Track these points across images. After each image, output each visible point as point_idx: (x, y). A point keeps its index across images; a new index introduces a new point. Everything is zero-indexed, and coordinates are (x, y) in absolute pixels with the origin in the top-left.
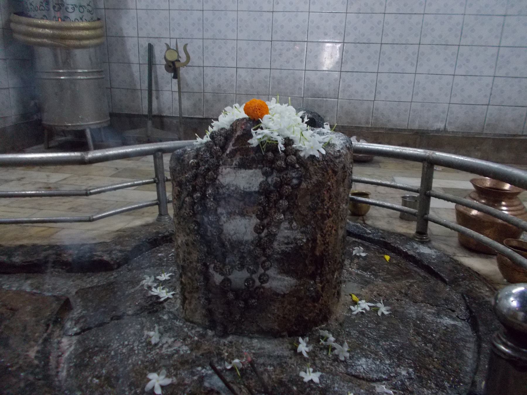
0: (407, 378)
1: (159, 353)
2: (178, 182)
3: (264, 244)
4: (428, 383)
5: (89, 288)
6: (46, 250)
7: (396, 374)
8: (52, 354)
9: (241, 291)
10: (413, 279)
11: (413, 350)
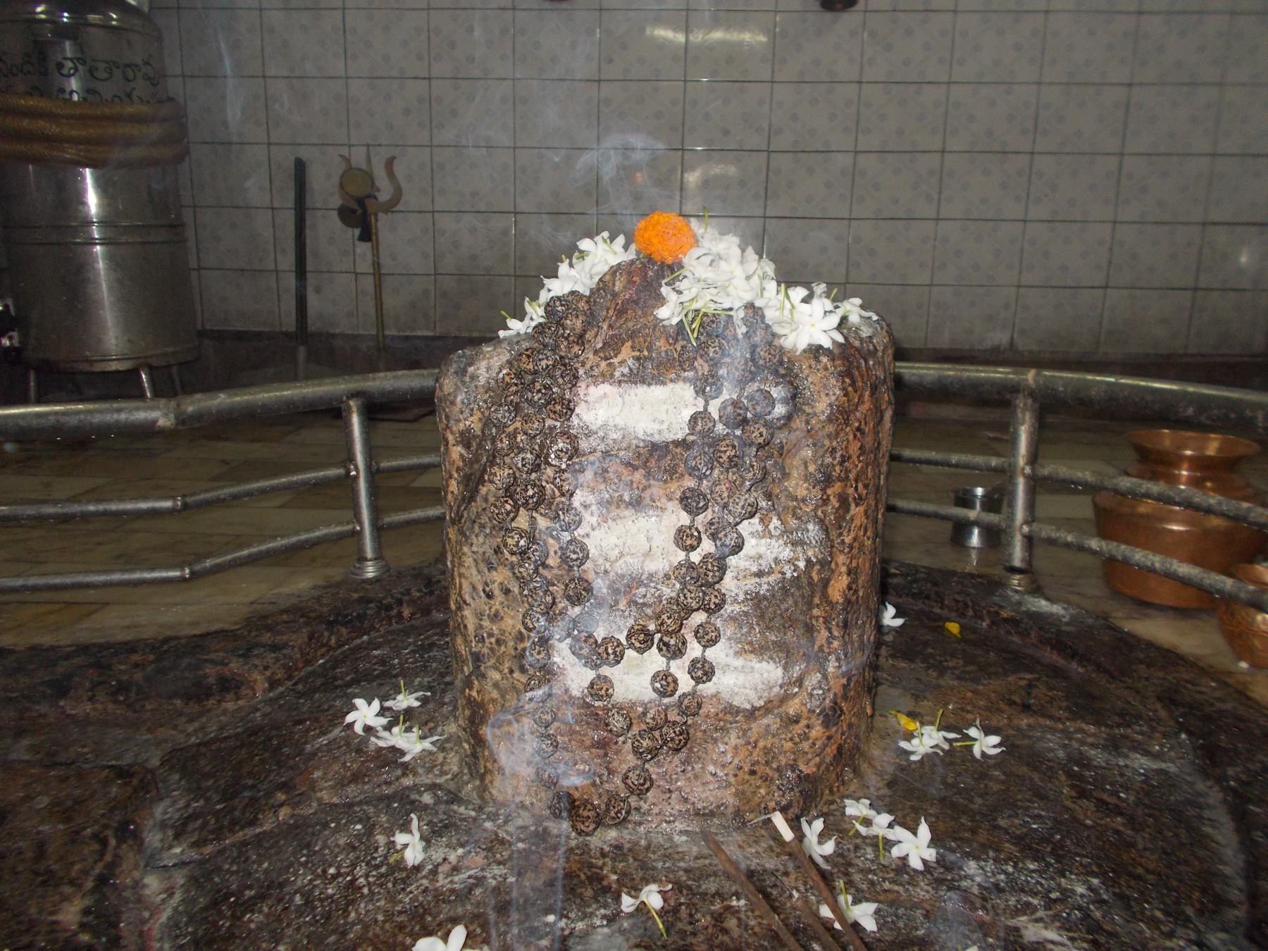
0: (1093, 903)
1: (431, 888)
2: (462, 433)
3: (705, 574)
4: (1145, 908)
5: (199, 744)
6: (68, 657)
7: (1061, 894)
8: (124, 917)
9: (640, 709)
10: (1031, 673)
11: (1086, 834)
